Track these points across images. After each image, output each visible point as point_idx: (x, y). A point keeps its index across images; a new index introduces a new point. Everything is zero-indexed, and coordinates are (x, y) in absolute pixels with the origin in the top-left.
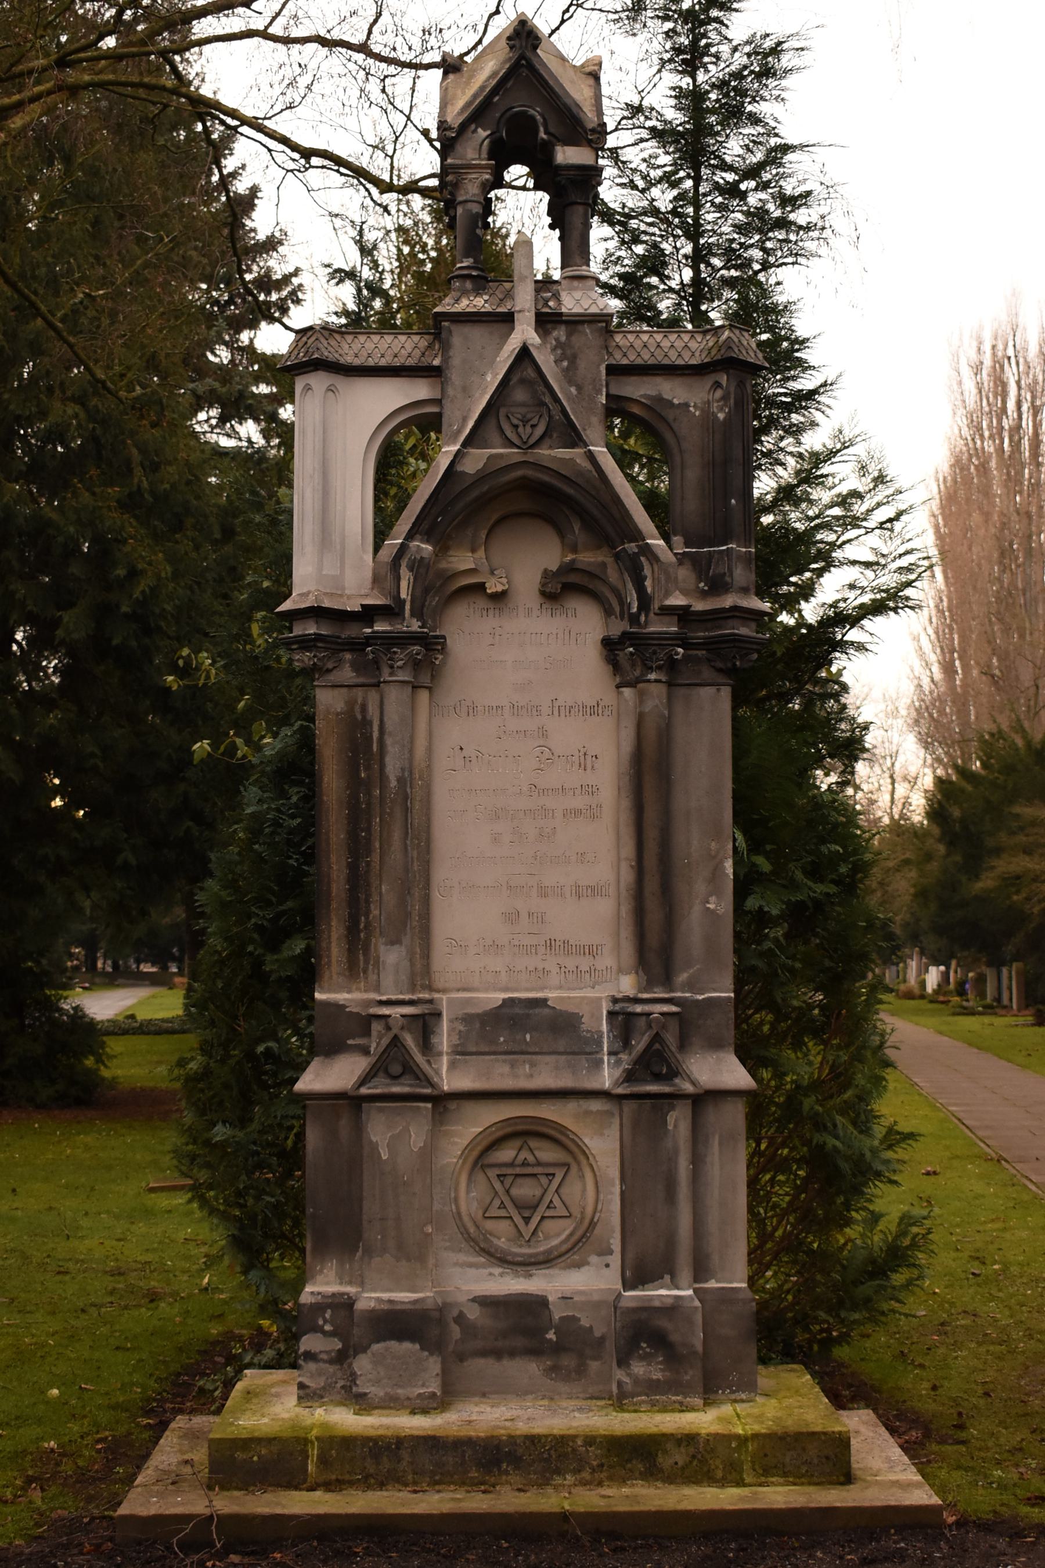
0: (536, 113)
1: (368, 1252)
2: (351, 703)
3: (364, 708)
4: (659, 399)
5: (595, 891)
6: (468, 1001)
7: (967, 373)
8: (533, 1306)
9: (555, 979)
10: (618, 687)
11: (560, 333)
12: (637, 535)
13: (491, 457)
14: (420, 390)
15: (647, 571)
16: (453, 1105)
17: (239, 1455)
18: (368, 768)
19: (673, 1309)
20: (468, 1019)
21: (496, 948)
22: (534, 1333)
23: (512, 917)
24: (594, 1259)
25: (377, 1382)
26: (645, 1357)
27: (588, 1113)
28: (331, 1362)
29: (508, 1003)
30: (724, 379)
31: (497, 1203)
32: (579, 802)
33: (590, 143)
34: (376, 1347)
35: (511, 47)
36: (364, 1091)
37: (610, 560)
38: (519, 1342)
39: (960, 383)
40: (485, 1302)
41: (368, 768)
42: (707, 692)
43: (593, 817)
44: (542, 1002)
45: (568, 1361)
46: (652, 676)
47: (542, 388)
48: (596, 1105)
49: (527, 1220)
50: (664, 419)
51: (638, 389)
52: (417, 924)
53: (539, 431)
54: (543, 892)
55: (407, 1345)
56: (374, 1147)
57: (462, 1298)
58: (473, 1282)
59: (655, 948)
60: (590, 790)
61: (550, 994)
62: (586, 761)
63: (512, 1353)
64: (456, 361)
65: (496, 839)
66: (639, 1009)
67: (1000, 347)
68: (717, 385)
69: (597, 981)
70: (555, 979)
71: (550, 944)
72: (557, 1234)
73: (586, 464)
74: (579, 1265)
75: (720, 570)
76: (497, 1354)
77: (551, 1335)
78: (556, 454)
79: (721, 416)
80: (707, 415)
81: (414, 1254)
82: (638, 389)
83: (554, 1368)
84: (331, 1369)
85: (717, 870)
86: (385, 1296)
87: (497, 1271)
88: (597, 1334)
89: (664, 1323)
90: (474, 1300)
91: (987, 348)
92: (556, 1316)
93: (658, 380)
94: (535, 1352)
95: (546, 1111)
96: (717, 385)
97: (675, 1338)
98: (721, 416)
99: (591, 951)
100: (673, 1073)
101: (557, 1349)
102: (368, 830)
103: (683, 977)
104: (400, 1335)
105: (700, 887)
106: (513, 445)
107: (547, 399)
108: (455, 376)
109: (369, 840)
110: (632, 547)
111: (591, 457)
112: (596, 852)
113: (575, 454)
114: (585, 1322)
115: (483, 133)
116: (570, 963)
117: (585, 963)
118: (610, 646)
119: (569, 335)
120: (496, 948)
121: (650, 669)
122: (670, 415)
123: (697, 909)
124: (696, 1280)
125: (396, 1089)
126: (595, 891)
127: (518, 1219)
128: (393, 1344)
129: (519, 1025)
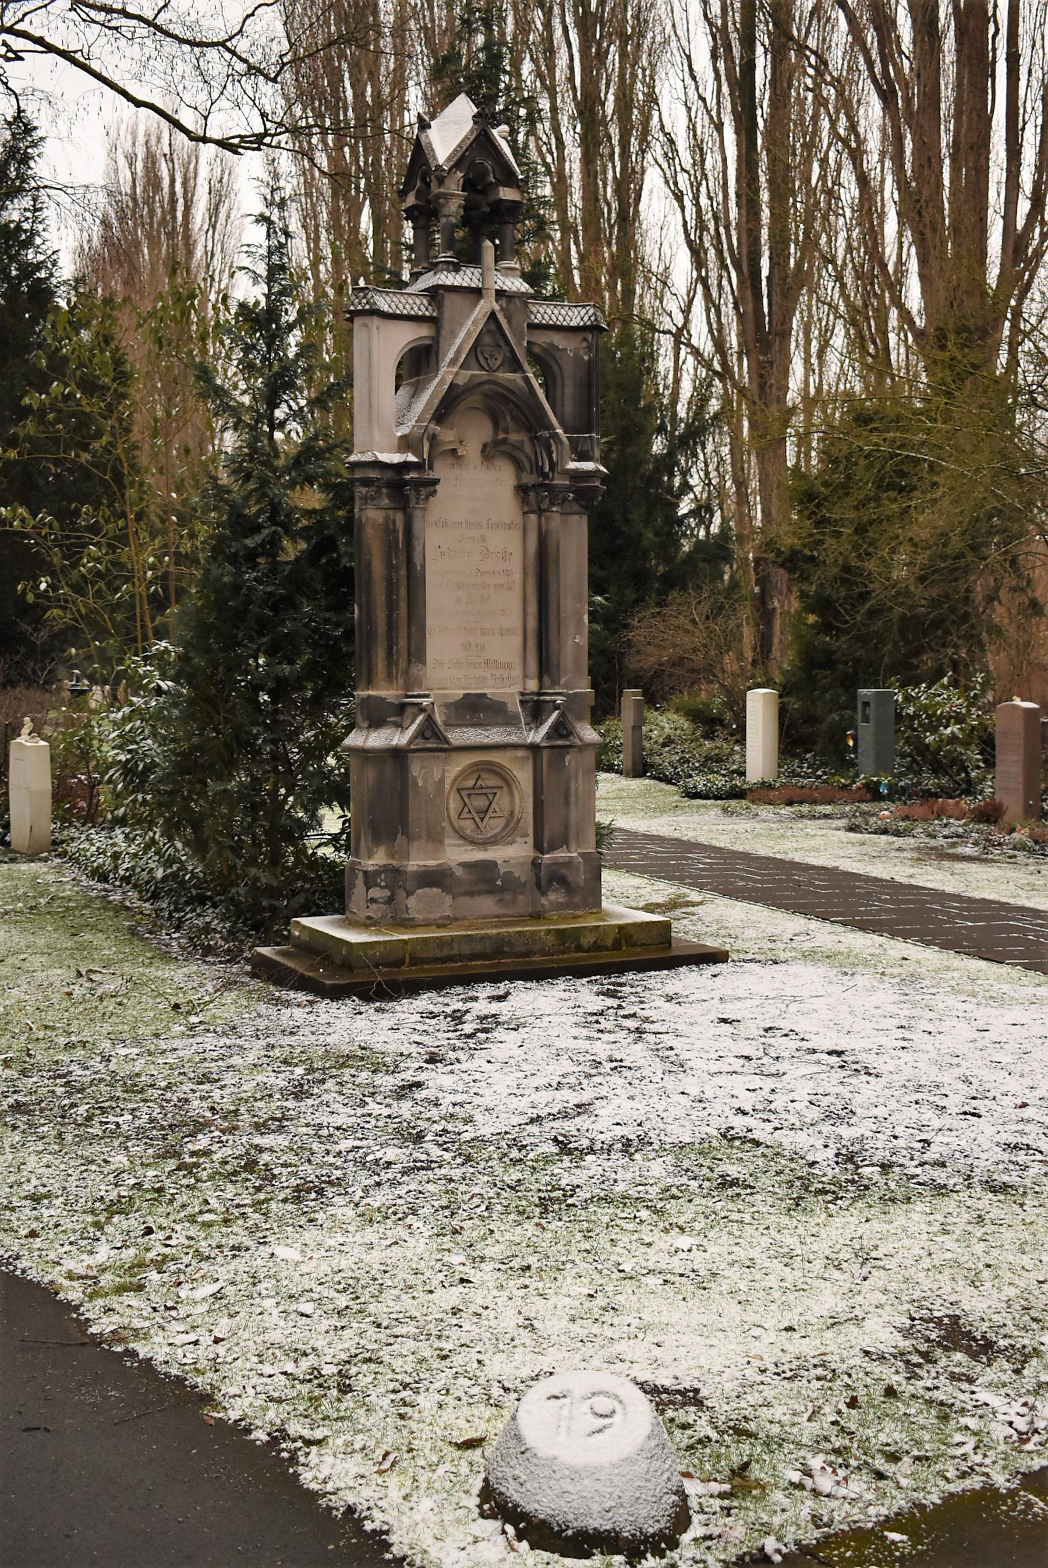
0: (488, 164)
1: (409, 837)
2: (387, 519)
3: (394, 522)
4: (552, 345)
5: (510, 631)
6: (445, 695)
7: (122, 162)
8: (488, 867)
9: (490, 682)
10: (525, 513)
11: (503, 302)
12: (550, 427)
13: (472, 376)
14: (424, 331)
15: (554, 448)
16: (454, 755)
17: (370, 952)
18: (397, 558)
19: (569, 863)
20: (447, 706)
21: (458, 664)
22: (491, 882)
23: (467, 647)
24: (519, 839)
25: (418, 912)
26: (556, 890)
27: (516, 757)
28: (385, 903)
29: (466, 695)
30: (590, 337)
31: (466, 810)
32: (502, 580)
33: (518, 187)
34: (419, 891)
35: (475, 123)
36: (412, 747)
37: (526, 439)
38: (483, 887)
39: (116, 171)
40: (465, 865)
41: (397, 558)
42: (576, 518)
43: (509, 589)
44: (483, 696)
45: (508, 896)
46: (554, 509)
47: (499, 336)
48: (520, 753)
49: (482, 819)
50: (554, 358)
51: (542, 339)
52: (417, 653)
53: (499, 362)
54: (483, 632)
55: (435, 890)
56: (415, 779)
57: (453, 864)
58: (457, 854)
59: (546, 665)
60: (507, 573)
61: (487, 691)
62: (506, 556)
63: (479, 893)
64: (446, 315)
65: (458, 601)
66: (548, 698)
67: (153, 142)
68: (585, 339)
69: (509, 682)
70: (490, 682)
71: (487, 662)
72: (494, 825)
73: (522, 383)
74: (511, 843)
75: (585, 448)
76: (471, 894)
77: (499, 883)
78: (506, 376)
79: (586, 358)
80: (577, 358)
81: (436, 839)
82: (542, 339)
83: (500, 901)
84: (385, 907)
85: (580, 620)
86: (421, 863)
87: (470, 848)
88: (523, 880)
89: (564, 871)
90: (459, 864)
91: (141, 139)
92: (502, 871)
93: (551, 333)
94: (490, 892)
95: (495, 757)
96: (585, 339)
97: (570, 879)
98: (586, 358)
99: (509, 666)
100: (570, 734)
101: (503, 890)
102: (398, 595)
103: (563, 681)
104: (431, 884)
105: (572, 630)
106: (483, 369)
107: (502, 343)
108: (446, 325)
109: (398, 601)
110: (546, 434)
111: (527, 380)
112: (509, 609)
113: (517, 377)
114: (516, 875)
115: (460, 175)
116: (498, 673)
117: (505, 673)
118: (522, 490)
119: (508, 303)
120: (458, 664)
121: (553, 505)
122: (557, 354)
123: (570, 642)
124: (578, 846)
125: (429, 746)
126: (510, 631)
127: (477, 819)
128: (427, 890)
129: (475, 708)
